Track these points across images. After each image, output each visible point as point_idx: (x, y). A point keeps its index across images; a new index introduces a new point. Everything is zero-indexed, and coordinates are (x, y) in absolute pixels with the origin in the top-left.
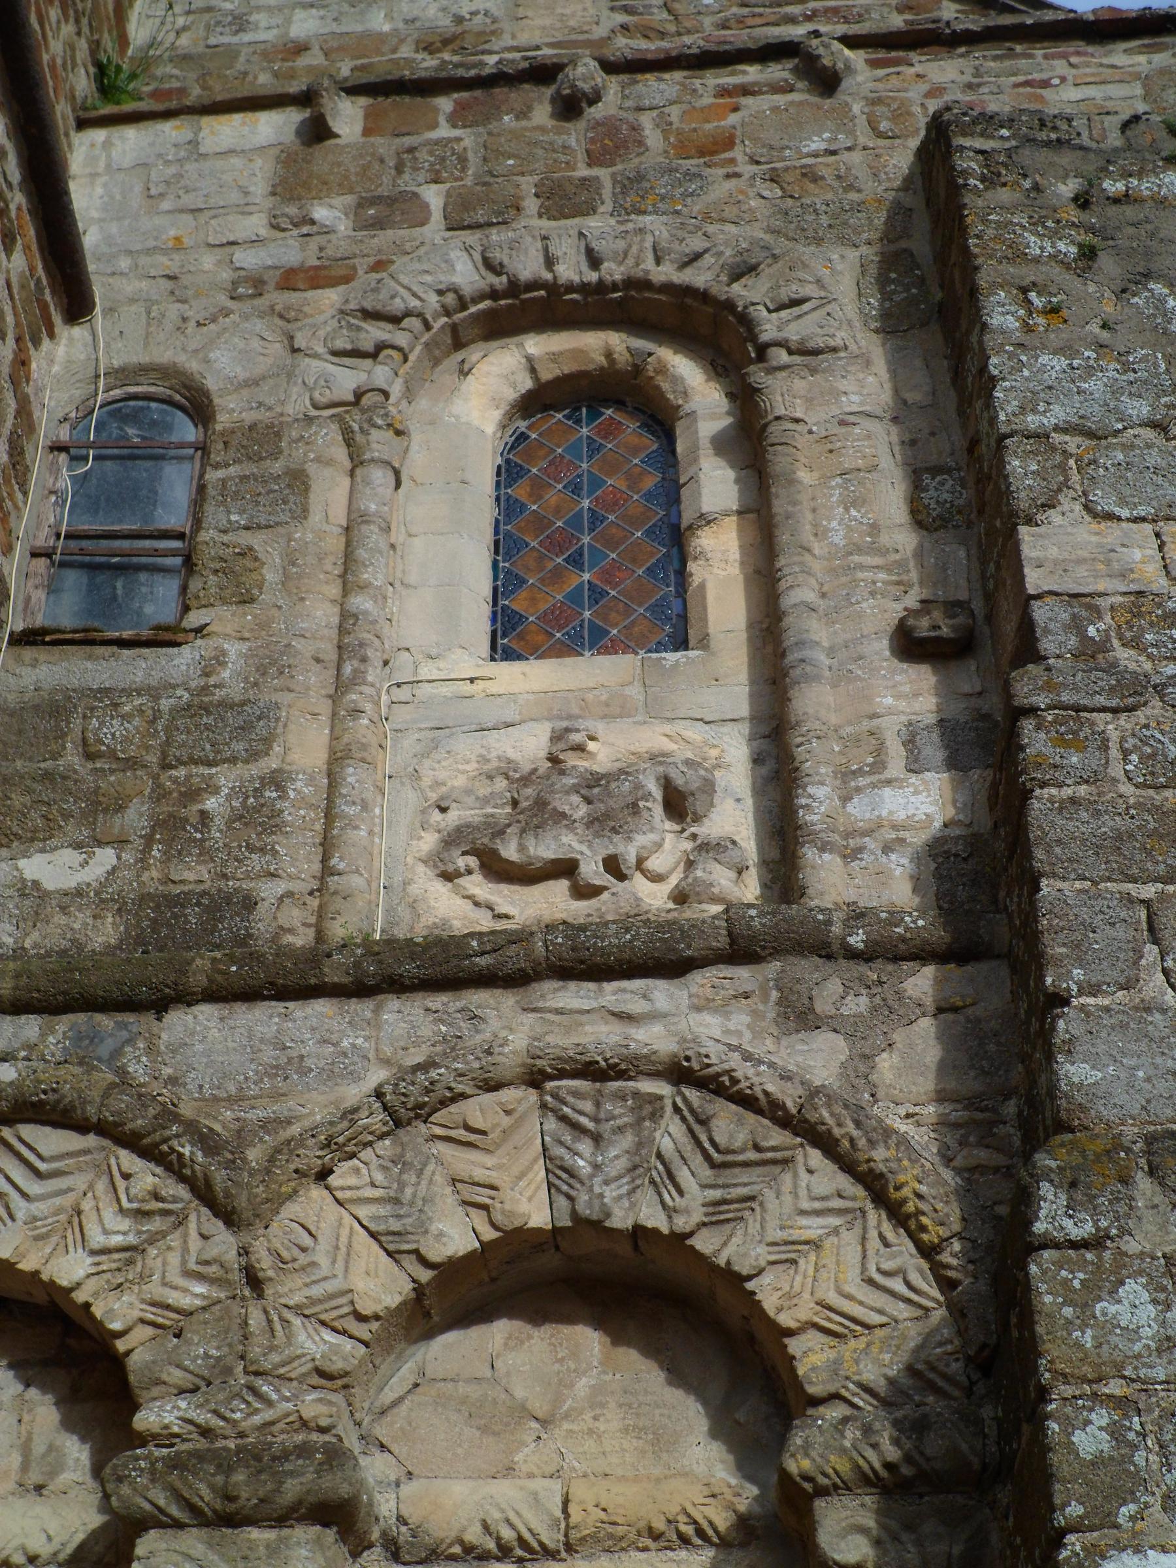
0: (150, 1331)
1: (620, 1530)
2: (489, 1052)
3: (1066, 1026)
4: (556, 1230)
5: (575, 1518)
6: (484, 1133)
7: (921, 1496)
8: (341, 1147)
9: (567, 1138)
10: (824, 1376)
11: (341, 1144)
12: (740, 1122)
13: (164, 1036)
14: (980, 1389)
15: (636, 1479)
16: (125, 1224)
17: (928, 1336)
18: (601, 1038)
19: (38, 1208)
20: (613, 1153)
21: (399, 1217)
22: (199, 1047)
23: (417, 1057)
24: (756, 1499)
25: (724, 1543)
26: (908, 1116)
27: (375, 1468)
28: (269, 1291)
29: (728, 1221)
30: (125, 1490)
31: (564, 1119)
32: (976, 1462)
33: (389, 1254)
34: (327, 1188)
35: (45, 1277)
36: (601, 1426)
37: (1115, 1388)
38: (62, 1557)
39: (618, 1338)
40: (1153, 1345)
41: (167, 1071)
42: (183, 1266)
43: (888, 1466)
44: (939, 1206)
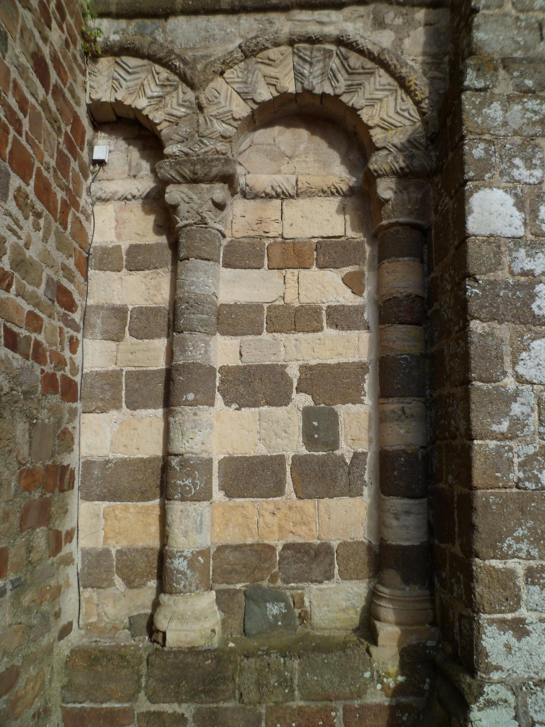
0: (167, 124)
1: (313, 190)
2: (276, 33)
3: (477, 19)
4: (297, 94)
5: (300, 185)
6: (274, 61)
7: (410, 179)
8: (228, 64)
9: (301, 64)
10: (381, 141)
11: (228, 63)
12: (358, 59)
13: (168, 27)
14: (430, 147)
15: (318, 175)
16: (158, 89)
17: (414, 131)
18: (314, 29)
19: (130, 84)
20: (316, 69)
21: (247, 88)
22: (180, 31)
23: (252, 35)
24: (355, 182)
25: (345, 195)
26: (413, 60)
27: (240, 170)
28: (205, 111)
29: (353, 92)
30: (162, 171)
31: (300, 57)
32: (429, 168)
33: (244, 100)
34: (223, 78)
35: (133, 106)
36: (308, 159)
37: (487, 137)
38: (143, 196)
39: (313, 132)
40: (501, 124)
41: (169, 39)
42: (178, 101)
43: (401, 169)
44: (422, 88)
